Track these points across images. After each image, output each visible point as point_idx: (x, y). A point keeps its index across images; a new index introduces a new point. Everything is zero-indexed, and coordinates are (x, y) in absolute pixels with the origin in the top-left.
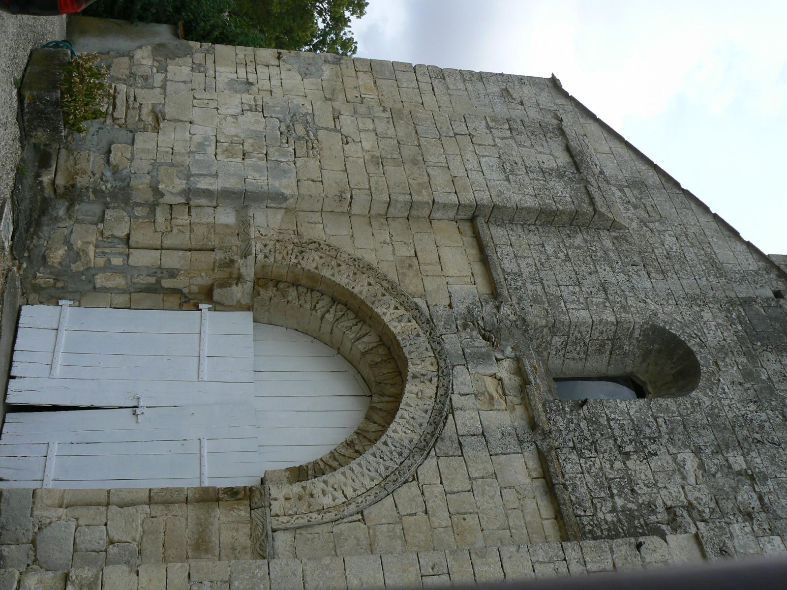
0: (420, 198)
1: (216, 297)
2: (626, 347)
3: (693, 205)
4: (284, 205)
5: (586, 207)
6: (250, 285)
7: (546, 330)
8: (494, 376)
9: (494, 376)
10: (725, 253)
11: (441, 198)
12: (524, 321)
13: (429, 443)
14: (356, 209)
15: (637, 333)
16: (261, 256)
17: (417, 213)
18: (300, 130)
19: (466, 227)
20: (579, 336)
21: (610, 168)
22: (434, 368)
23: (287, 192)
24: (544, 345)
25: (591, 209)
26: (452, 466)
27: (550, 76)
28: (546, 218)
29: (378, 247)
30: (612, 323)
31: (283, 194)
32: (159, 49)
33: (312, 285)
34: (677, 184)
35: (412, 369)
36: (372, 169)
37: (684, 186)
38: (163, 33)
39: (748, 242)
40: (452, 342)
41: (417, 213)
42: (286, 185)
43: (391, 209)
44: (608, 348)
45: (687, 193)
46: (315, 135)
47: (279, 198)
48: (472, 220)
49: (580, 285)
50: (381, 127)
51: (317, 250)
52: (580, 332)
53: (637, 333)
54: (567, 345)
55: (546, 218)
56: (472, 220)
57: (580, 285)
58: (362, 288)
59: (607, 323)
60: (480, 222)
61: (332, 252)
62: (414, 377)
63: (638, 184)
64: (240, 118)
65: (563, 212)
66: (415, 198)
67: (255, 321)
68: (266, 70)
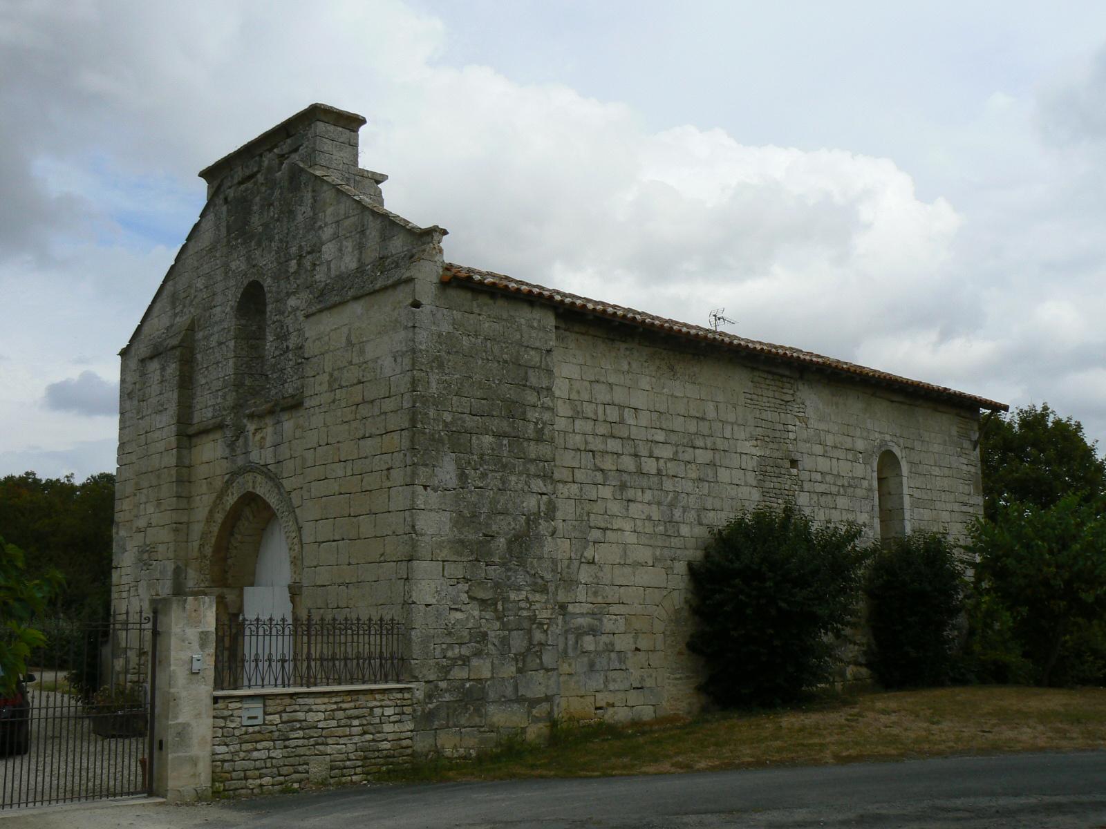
0: (175, 475)
1: (235, 611)
2: (254, 328)
3: (183, 257)
4: (183, 567)
5: (177, 353)
6: (225, 590)
7: (241, 391)
8: (254, 434)
9: (254, 434)
10: (206, 238)
11: (173, 461)
12: (233, 408)
13: (274, 480)
14: (185, 519)
15: (243, 322)
16: (207, 584)
17: (184, 476)
18: (145, 556)
19: (194, 440)
20: (244, 366)
21: (165, 321)
22: (251, 474)
23: (173, 566)
24: (251, 391)
25: (179, 349)
26: (289, 466)
27: (119, 357)
28: (186, 383)
29: (203, 502)
30: (236, 342)
31: (174, 570)
32: (115, 656)
33: (222, 550)
34: (173, 267)
35: (251, 490)
36: (163, 508)
37: (173, 263)
38: (106, 651)
39: (176, 260)
40: (240, 461)
41: (184, 476)
42: (170, 566)
43: (183, 495)
44: (253, 342)
45: (177, 259)
46: (148, 545)
47: (178, 572)
48: (190, 437)
49: (218, 363)
50: (143, 499)
51: (204, 547)
52: (242, 366)
53: (243, 322)
54: (252, 374)
55: (186, 383)
56: (190, 437)
57: (218, 363)
58: (219, 517)
59: (235, 347)
60: (191, 430)
61: (204, 536)
62: (254, 488)
63: (174, 299)
64: (141, 597)
65: (181, 371)
66: (174, 480)
67: (252, 585)
68: (124, 577)
